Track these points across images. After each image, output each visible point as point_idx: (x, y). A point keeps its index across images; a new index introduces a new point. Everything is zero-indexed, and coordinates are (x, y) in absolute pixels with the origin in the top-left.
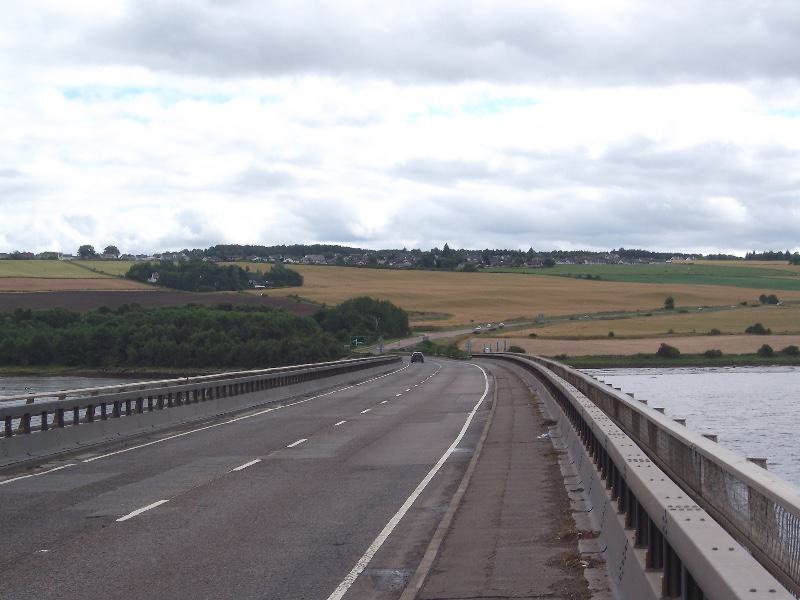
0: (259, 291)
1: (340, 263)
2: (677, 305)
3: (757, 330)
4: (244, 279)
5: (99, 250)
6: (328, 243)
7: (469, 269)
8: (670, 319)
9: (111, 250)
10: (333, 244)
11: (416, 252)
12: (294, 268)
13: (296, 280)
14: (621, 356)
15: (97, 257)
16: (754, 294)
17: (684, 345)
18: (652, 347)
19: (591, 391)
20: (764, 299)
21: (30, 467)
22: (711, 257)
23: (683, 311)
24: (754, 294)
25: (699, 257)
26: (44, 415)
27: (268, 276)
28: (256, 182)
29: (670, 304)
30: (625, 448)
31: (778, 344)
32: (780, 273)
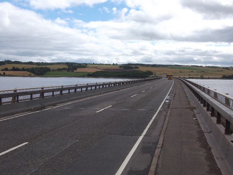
0: (134, 69)
1: (142, 66)
2: (181, 72)
3: (189, 75)
4: (131, 68)
5: (115, 64)
6: (208, 65)
7: (158, 67)
8: (180, 74)
9: (117, 64)
10: (199, 65)
11: (151, 65)
12: (138, 66)
13: (138, 68)
14: (46, 77)
15: (115, 65)
16: (190, 71)
17: (205, 76)
18: (200, 76)
19: (186, 81)
20: (192, 71)
21: (118, 90)
22: (187, 66)
23: (182, 73)
24: (190, 71)
25: (185, 66)
26: (106, 85)
27: (135, 67)
28: (107, 55)
29: (181, 72)
30: (194, 87)
31: (191, 77)
32: (195, 68)
